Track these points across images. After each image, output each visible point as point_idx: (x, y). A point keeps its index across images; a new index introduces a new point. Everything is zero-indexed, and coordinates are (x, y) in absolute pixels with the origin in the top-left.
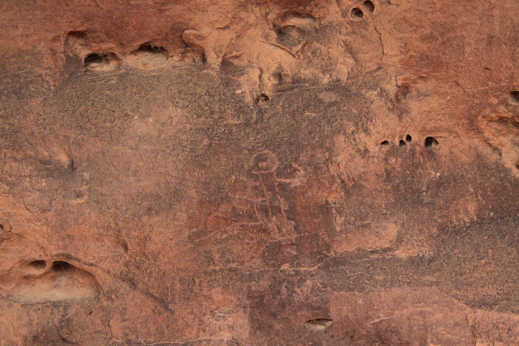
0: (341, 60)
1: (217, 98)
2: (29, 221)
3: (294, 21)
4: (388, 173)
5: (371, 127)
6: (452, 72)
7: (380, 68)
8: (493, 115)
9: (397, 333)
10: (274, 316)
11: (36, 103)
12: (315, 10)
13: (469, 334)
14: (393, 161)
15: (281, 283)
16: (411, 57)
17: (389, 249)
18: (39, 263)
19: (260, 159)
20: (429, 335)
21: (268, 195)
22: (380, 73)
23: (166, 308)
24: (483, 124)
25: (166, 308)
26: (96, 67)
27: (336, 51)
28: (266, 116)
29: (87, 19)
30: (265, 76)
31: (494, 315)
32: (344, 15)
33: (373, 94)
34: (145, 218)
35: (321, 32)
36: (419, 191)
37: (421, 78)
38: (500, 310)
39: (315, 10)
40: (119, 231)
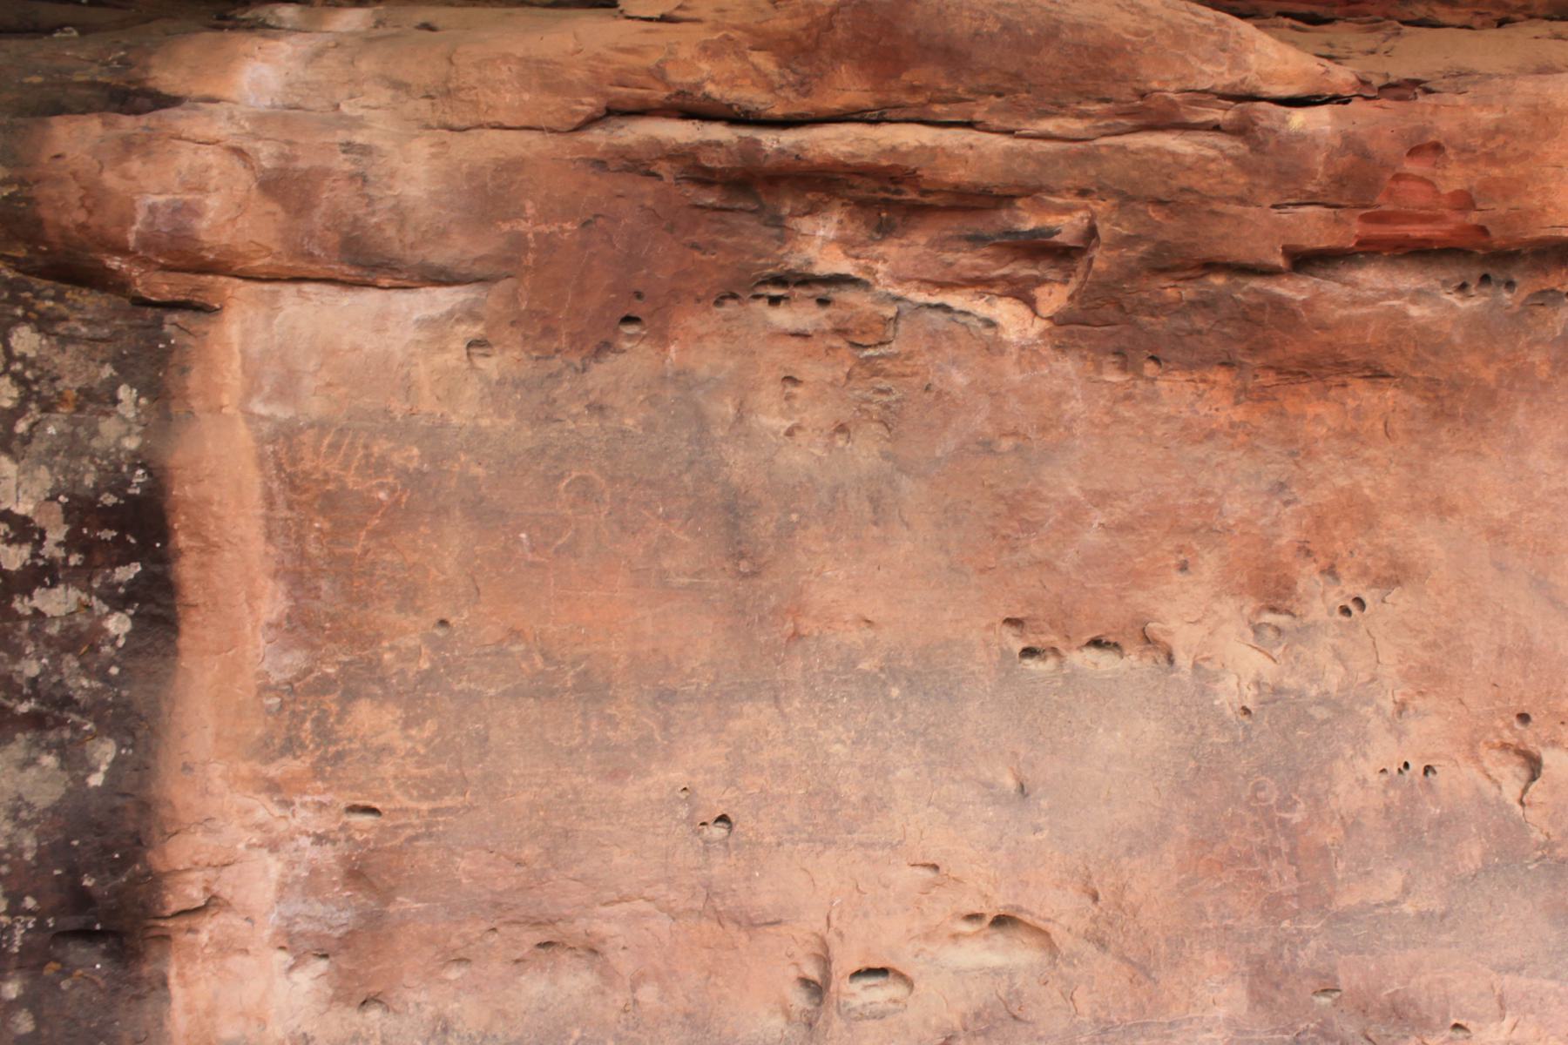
0: (1329, 667)
1: (1194, 709)
2: (972, 862)
3: (1269, 618)
4: (1388, 808)
5: (1369, 752)
6: (1456, 688)
7: (1373, 680)
8: (1496, 741)
9: (1416, 1007)
10: (1277, 986)
11: (972, 707)
12: (1296, 605)
13: (1496, 1005)
14: (1391, 793)
15: (1282, 944)
16: (1411, 667)
17: (1395, 903)
18: (973, 917)
19: (1258, 787)
20: (1452, 1008)
21: (1268, 831)
22: (1374, 685)
23: (1148, 976)
24: (1482, 750)
25: (1148, 976)
26: (1031, 664)
27: (1323, 657)
28: (1254, 734)
29: (1030, 602)
30: (1244, 684)
31: (1523, 982)
32: (1330, 613)
33: (1368, 711)
34: (1125, 860)
35: (1305, 632)
36: (1418, 832)
37: (1421, 693)
38: (1531, 976)
39: (1296, 605)
40: (1089, 877)
